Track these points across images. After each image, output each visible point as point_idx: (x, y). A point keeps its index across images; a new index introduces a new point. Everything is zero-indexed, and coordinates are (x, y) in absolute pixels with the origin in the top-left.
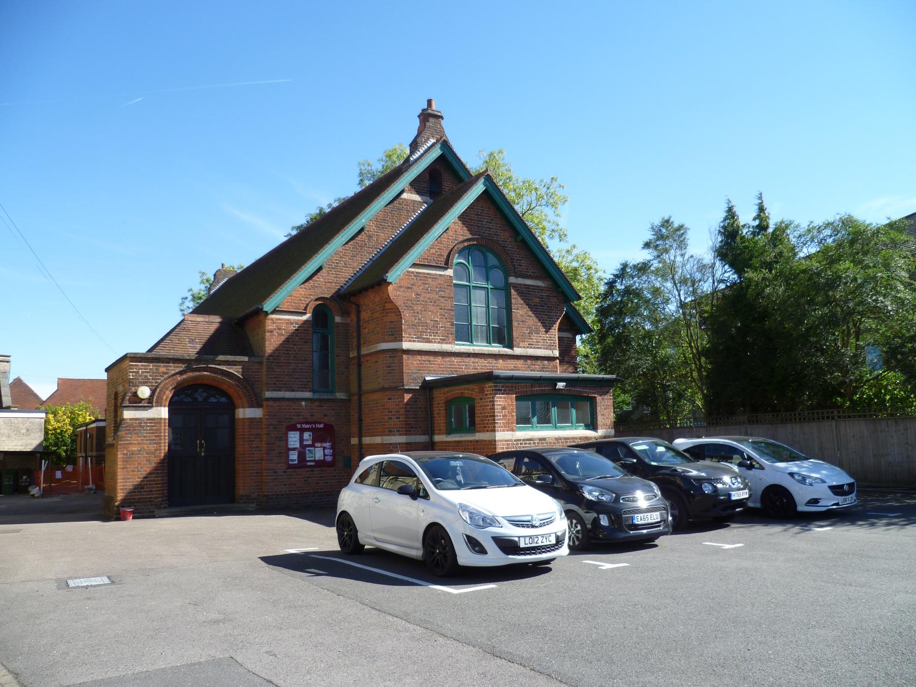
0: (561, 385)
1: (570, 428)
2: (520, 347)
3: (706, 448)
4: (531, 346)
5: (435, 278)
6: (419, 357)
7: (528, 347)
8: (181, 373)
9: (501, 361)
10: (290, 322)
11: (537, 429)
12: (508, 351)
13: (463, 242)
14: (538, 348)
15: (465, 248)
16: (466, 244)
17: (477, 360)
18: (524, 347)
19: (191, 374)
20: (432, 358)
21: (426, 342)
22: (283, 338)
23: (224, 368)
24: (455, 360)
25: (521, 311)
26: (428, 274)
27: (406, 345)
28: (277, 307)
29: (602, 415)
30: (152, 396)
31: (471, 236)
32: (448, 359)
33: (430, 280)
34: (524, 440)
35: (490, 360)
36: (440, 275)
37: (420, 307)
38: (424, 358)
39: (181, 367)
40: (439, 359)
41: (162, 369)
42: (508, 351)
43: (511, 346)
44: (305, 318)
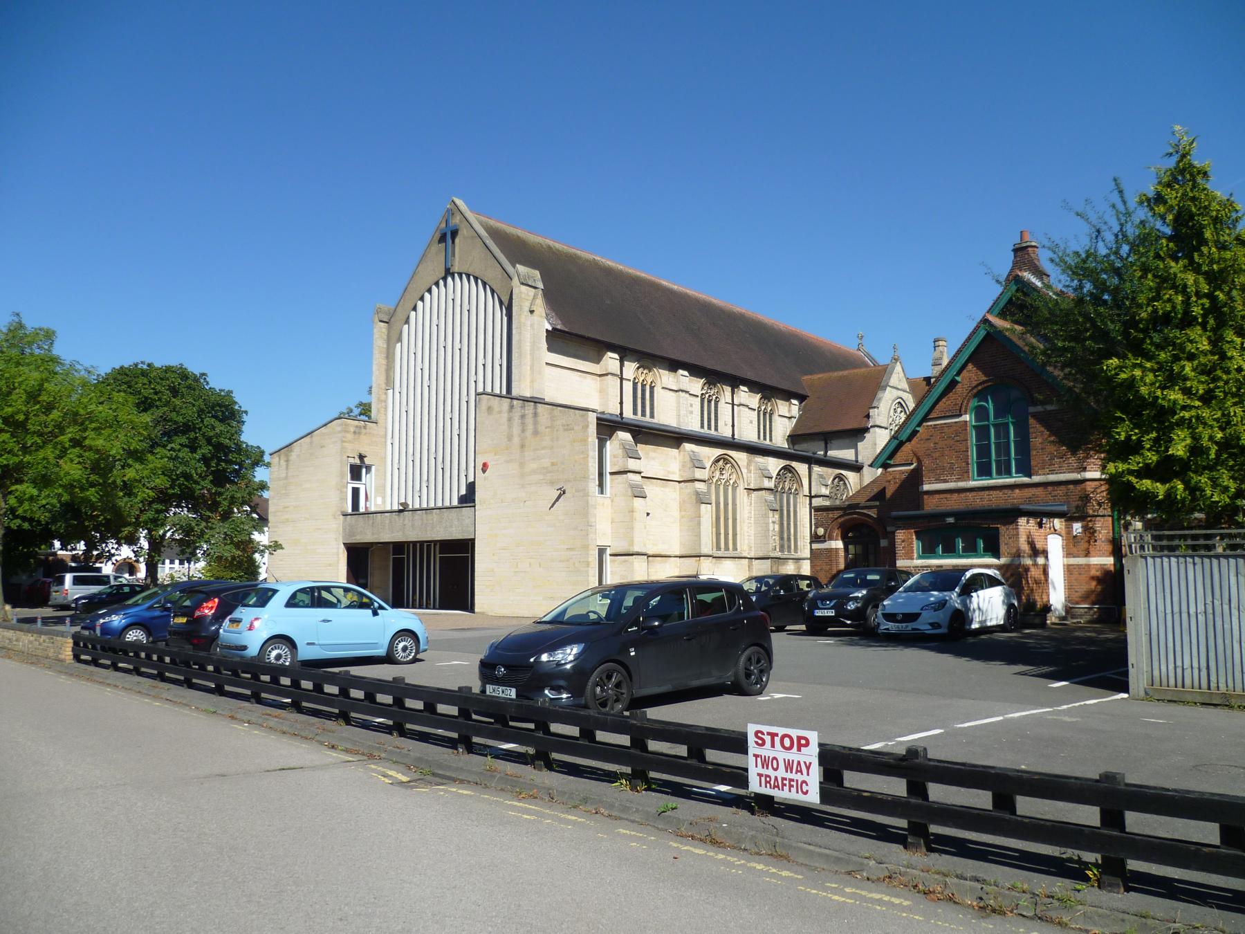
0: (951, 520)
1: (976, 557)
2: (1040, 475)
3: (418, 545)
4: (1052, 472)
5: (949, 425)
6: (937, 496)
7: (1048, 474)
8: (840, 517)
9: (1017, 491)
10: (902, 472)
11: (982, 556)
12: (1026, 480)
13: (976, 387)
14: (1061, 473)
15: (979, 392)
16: (980, 388)
17: (991, 492)
18: (1044, 474)
19: (846, 517)
20: (948, 496)
21: (944, 482)
22: (898, 485)
23: (865, 511)
24: (970, 495)
25: (1039, 436)
26: (945, 424)
27: (926, 487)
28: (328, 589)
29: (1006, 544)
30: (825, 533)
31: (985, 378)
32: (963, 495)
33: (946, 430)
34: (921, 567)
35: (1006, 491)
36: (956, 422)
37: (937, 454)
38: (942, 496)
39: (841, 513)
40: (955, 496)
41: (831, 516)
42: (1026, 480)
43: (1030, 476)
44: (912, 467)
